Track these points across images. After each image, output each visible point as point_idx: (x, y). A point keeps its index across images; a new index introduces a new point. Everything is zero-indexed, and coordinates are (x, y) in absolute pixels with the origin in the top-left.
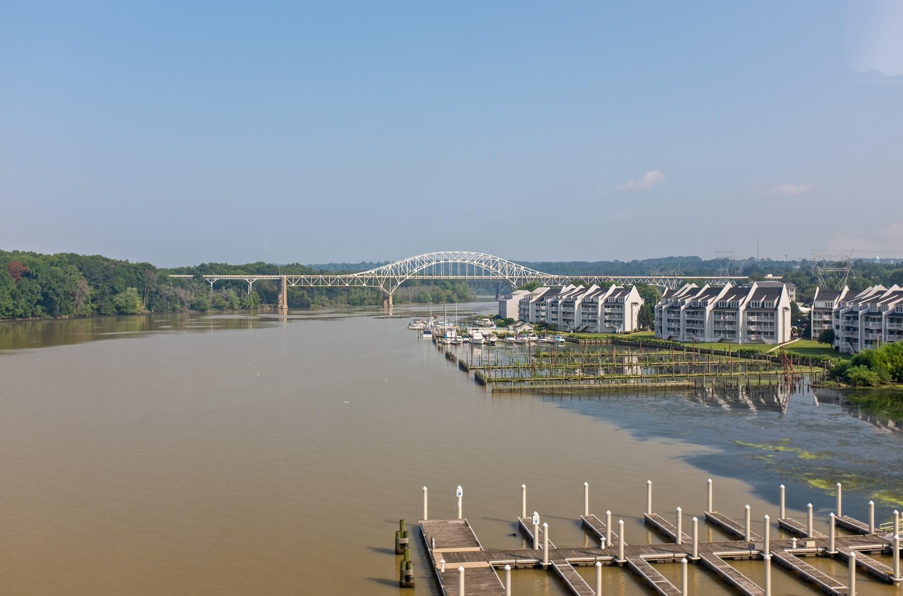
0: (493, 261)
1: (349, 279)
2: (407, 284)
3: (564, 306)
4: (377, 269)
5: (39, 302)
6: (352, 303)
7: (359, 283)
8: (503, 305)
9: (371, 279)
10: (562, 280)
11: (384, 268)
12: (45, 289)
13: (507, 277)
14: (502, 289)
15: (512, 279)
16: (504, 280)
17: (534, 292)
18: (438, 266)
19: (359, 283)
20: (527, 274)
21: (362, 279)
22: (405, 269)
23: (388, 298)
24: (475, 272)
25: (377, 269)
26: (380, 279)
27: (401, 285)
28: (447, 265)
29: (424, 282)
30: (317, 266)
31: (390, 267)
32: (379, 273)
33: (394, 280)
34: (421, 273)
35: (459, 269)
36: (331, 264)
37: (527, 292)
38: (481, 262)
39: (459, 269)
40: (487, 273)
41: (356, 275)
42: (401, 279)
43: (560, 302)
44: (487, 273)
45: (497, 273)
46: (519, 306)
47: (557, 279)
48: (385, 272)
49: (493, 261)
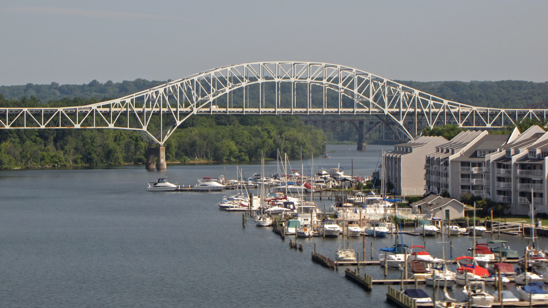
0: (360, 80)
1: (83, 114)
2: (191, 122)
3: (523, 166)
4: (135, 96)
5: (170, 287)
6: (88, 162)
7: (30, 122)
8: (394, 164)
9: (124, 114)
10: (493, 115)
11: (150, 92)
12: (339, 129)
13: (386, 111)
14: (387, 132)
15: (396, 114)
16: (380, 116)
17: (454, 140)
18: (253, 89)
19: (65, 122)
20: (425, 104)
21: (107, 114)
22: (189, 91)
23: (156, 151)
24: (309, 101)
25: (135, 96)
26: (141, 114)
27: (182, 126)
28: (271, 86)
29: (220, 120)
30: (14, 89)
31: (161, 91)
32: (139, 102)
33: (168, 115)
34: (221, 102)
35: (278, 97)
36: (29, 86)
37: (441, 141)
38: (336, 81)
39: (278, 97)
40: (348, 103)
41: (94, 106)
42: (183, 115)
43: (514, 159)
44: (348, 103)
45: (367, 104)
46: (426, 167)
47: (484, 115)
48: (151, 102)
49: (360, 80)
